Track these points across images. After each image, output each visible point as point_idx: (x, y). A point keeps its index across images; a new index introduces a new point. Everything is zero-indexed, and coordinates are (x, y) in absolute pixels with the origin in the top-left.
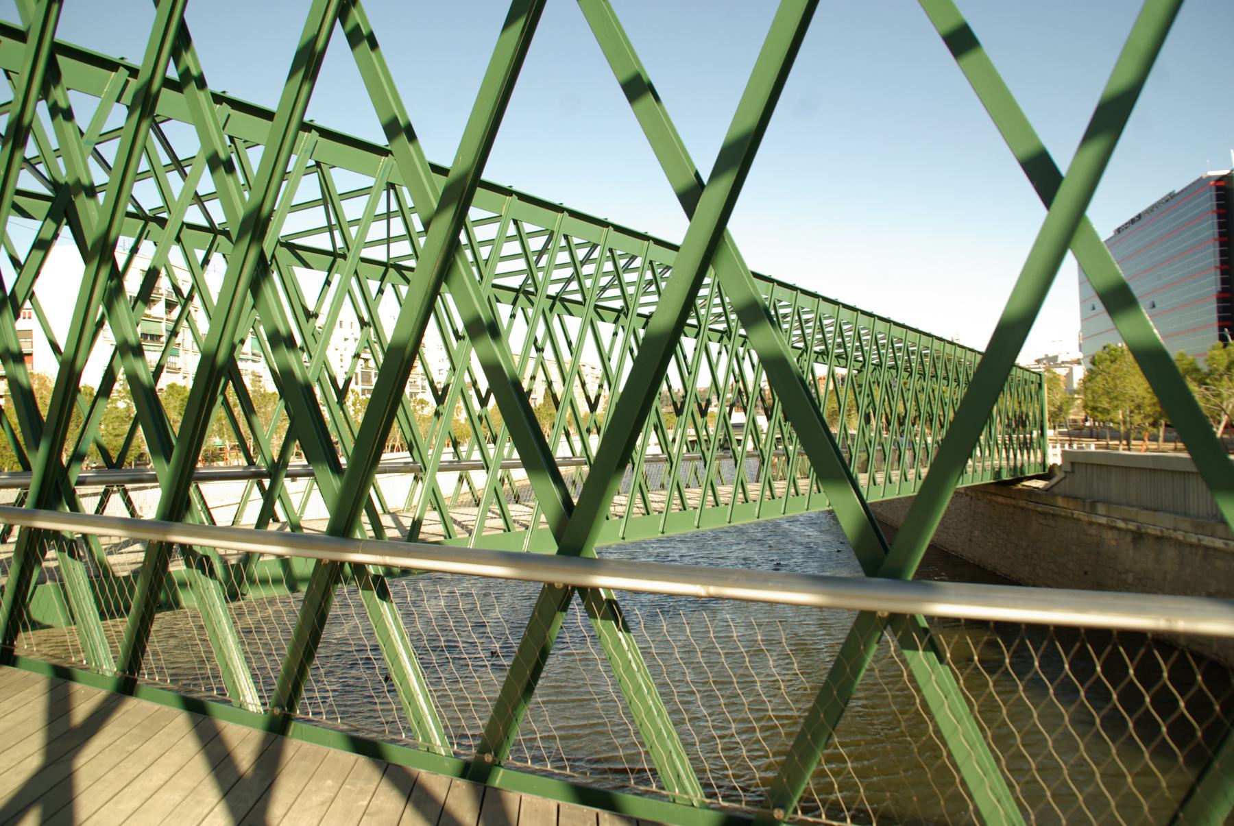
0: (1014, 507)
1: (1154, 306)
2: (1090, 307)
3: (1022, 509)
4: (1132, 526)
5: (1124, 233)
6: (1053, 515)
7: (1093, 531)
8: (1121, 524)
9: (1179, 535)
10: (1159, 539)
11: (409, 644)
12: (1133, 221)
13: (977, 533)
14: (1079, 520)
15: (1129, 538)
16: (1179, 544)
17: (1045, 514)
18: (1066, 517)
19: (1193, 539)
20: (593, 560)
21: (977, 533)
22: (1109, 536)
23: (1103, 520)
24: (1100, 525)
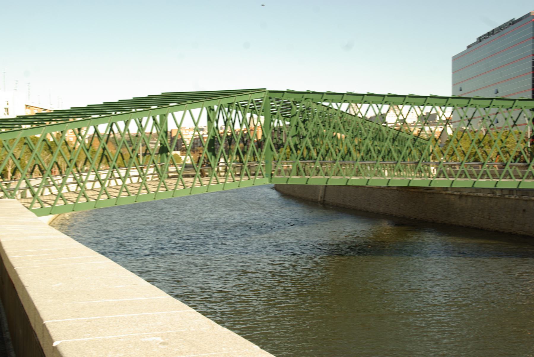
0: (418, 192)
1: (497, 92)
2: (459, 89)
3: (421, 192)
4: (459, 193)
5: (484, 42)
6: (433, 193)
7: (446, 197)
8: (455, 193)
9: (472, 194)
10: (467, 196)
11: (367, 111)
12: (489, 34)
13: (402, 205)
14: (442, 193)
15: (458, 197)
16: (472, 196)
17: (430, 193)
18: (438, 193)
19: (475, 194)
20: (443, 131)
21: (402, 205)
22: (452, 197)
23: (450, 192)
24: (449, 194)
